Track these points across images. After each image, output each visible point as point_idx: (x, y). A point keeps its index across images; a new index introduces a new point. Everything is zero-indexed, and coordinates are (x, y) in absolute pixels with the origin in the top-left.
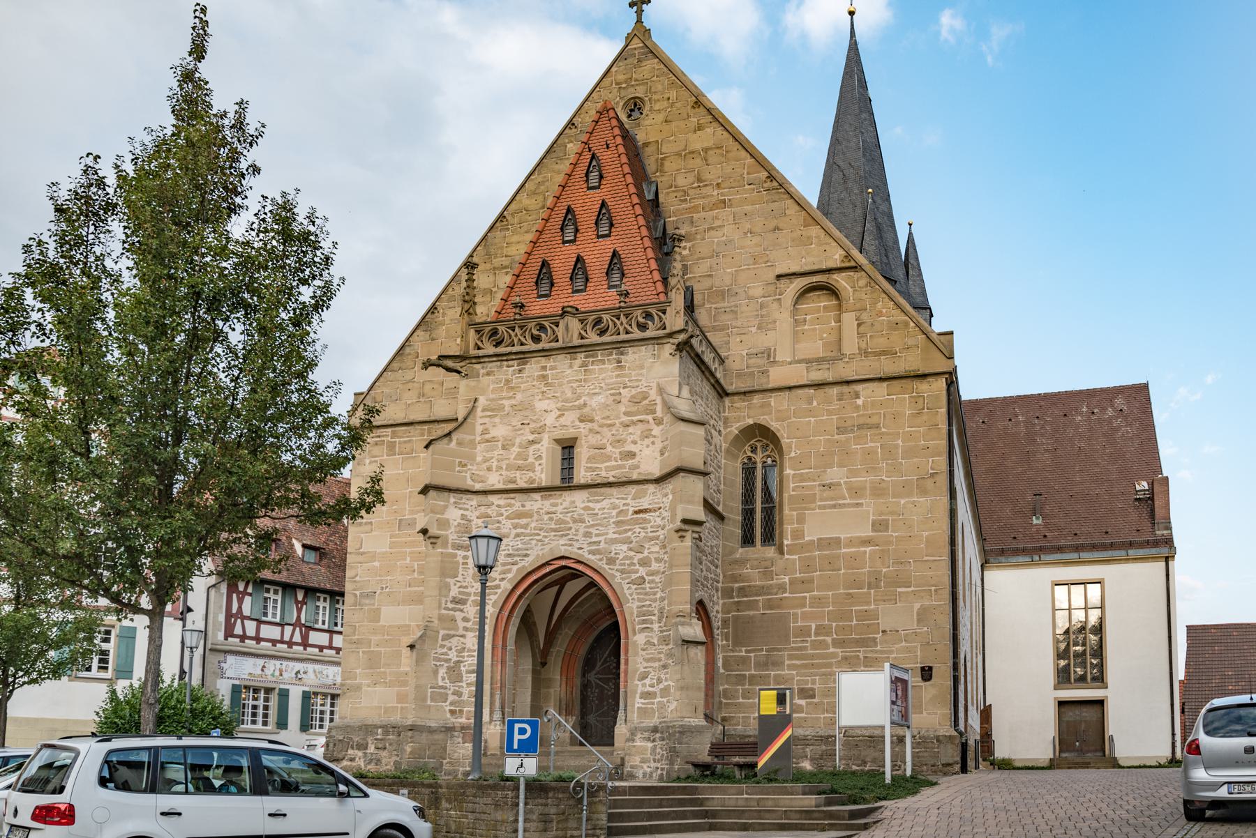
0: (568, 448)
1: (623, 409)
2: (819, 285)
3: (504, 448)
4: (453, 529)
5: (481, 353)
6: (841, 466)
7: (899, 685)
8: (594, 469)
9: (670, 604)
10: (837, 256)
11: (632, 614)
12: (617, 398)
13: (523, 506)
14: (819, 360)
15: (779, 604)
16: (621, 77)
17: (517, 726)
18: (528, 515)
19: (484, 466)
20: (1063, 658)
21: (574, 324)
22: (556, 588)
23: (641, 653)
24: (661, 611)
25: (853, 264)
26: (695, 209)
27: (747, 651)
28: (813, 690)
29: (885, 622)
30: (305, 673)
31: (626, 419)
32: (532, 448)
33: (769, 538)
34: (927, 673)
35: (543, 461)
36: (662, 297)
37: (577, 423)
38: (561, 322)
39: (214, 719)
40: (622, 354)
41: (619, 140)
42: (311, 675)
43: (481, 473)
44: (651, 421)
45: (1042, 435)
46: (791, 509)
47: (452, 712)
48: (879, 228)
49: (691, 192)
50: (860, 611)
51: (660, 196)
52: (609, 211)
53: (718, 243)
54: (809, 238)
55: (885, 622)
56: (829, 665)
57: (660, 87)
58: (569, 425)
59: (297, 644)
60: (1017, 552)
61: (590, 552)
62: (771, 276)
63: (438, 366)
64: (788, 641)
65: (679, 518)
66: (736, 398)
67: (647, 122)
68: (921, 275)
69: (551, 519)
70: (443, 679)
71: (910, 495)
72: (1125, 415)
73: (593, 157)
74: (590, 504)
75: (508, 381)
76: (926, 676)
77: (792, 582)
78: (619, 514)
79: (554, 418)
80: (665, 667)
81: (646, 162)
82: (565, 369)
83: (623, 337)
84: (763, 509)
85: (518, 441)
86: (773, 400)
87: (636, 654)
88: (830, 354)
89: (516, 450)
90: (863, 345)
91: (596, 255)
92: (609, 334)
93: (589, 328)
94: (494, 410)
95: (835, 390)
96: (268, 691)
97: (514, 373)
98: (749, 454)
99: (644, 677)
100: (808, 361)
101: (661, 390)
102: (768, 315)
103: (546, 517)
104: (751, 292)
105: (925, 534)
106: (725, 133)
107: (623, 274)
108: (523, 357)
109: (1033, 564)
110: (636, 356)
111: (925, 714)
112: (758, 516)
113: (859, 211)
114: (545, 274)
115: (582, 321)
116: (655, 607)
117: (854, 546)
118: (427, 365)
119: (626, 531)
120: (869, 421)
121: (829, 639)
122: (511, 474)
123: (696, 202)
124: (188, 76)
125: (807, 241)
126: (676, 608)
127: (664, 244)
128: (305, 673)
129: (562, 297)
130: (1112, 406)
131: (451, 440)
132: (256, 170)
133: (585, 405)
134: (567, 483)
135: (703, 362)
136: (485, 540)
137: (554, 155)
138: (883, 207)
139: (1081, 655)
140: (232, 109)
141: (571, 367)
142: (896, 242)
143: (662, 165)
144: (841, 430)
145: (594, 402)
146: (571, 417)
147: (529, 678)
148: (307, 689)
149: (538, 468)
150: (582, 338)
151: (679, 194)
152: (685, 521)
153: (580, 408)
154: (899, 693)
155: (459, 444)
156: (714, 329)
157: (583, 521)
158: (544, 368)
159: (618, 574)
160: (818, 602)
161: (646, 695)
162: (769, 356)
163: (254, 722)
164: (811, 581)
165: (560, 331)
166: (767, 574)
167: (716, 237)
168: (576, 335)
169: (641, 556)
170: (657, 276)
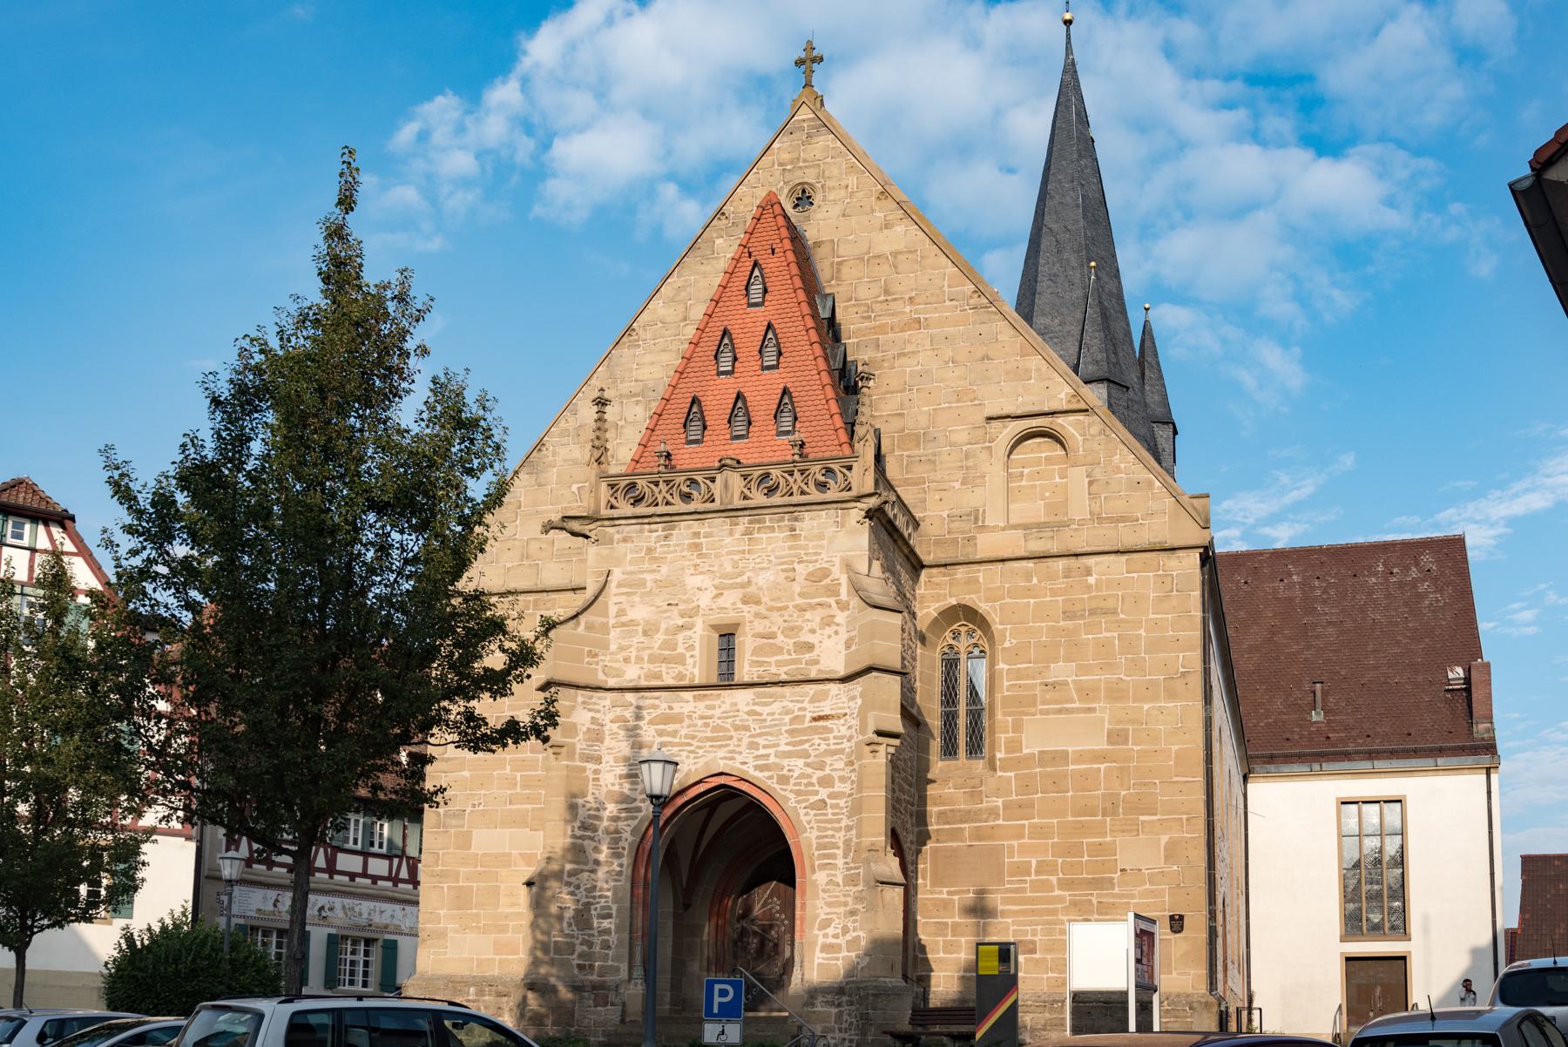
0: (727, 638)
1: (798, 590)
2: (1040, 430)
3: (645, 633)
4: (581, 736)
5: (615, 513)
6: (1068, 659)
7: (1144, 939)
8: (761, 664)
9: (859, 835)
10: (1062, 396)
11: (810, 846)
12: (790, 574)
13: (670, 708)
14: (1040, 526)
15: (991, 833)
16: (785, 156)
17: (717, 987)
18: (678, 719)
19: (620, 657)
20: (1352, 901)
21: (735, 480)
22: (705, 811)
23: (822, 895)
24: (847, 843)
25: (1084, 406)
26: (881, 329)
27: (949, 893)
28: (1033, 942)
29: (1125, 859)
30: (331, 909)
31: (800, 601)
32: (680, 637)
33: (975, 748)
34: (1177, 923)
35: (696, 652)
36: (846, 450)
37: (740, 605)
38: (718, 477)
39: (258, 972)
40: (796, 519)
41: (787, 244)
42: (339, 912)
43: (616, 665)
44: (834, 605)
45: (1324, 602)
46: (1005, 714)
47: (580, 967)
48: (1105, 315)
49: (877, 307)
50: (1093, 844)
51: (837, 310)
52: (775, 335)
53: (911, 374)
54: (1027, 371)
55: (1125, 859)
56: (1054, 912)
57: (835, 171)
58: (729, 607)
59: (404, 881)
60: (1288, 759)
61: (757, 768)
62: (979, 418)
63: (562, 529)
64: (1001, 881)
65: (871, 728)
66: (934, 570)
67: (819, 216)
68: (1161, 377)
69: (706, 725)
70: (570, 925)
71: (1155, 698)
72: (1439, 571)
73: (756, 264)
74: (756, 708)
75: (650, 550)
76: (1176, 927)
77: (1006, 806)
78: (793, 721)
79: (710, 599)
80: (853, 913)
81: (819, 267)
82: (723, 536)
83: (797, 499)
84: (970, 713)
85: (663, 626)
86: (981, 573)
87: (816, 896)
88: (1052, 519)
89: (660, 637)
90: (1096, 509)
91: (762, 392)
92: (777, 492)
93: (753, 485)
94: (633, 585)
95: (1061, 564)
96: (368, 942)
97: (658, 539)
98: (952, 642)
99: (826, 924)
100: (1026, 527)
101: (848, 567)
102: (975, 467)
103: (700, 722)
104: (954, 438)
105: (1175, 748)
106: (920, 233)
107: (796, 419)
108: (670, 518)
109: (1311, 774)
110: (815, 523)
111: (1174, 974)
112: (962, 721)
113: (1079, 293)
114: (695, 409)
115: (745, 477)
116: (840, 838)
117: (1083, 762)
118: (549, 527)
119: (802, 742)
120: (1103, 604)
121: (1054, 879)
122: (654, 668)
123: (884, 320)
124: (337, 233)
125: (1025, 375)
126: (866, 841)
127: (848, 383)
128: (331, 909)
129: (718, 445)
130: (1417, 565)
131: (578, 624)
132: (424, 351)
133: (749, 582)
134: (726, 680)
135: (896, 529)
136: (660, 765)
137: (698, 253)
138: (1110, 286)
139: (1375, 891)
140: (394, 277)
141: (731, 533)
142: (1128, 333)
143: (839, 271)
144: (1068, 615)
145: (764, 579)
146: (731, 598)
147: (670, 924)
148: (334, 931)
149: (690, 661)
150: (745, 498)
151: (861, 310)
152: (880, 733)
153: (742, 586)
154: (1145, 948)
155: (589, 628)
156: (907, 482)
157: (746, 728)
158: (697, 535)
159: (792, 796)
160: (1040, 832)
161: (827, 948)
162: (976, 519)
163: (352, 983)
164: (1031, 805)
165: (717, 488)
166: (975, 795)
167: (910, 366)
168: (737, 495)
169: (820, 774)
170: (838, 421)
